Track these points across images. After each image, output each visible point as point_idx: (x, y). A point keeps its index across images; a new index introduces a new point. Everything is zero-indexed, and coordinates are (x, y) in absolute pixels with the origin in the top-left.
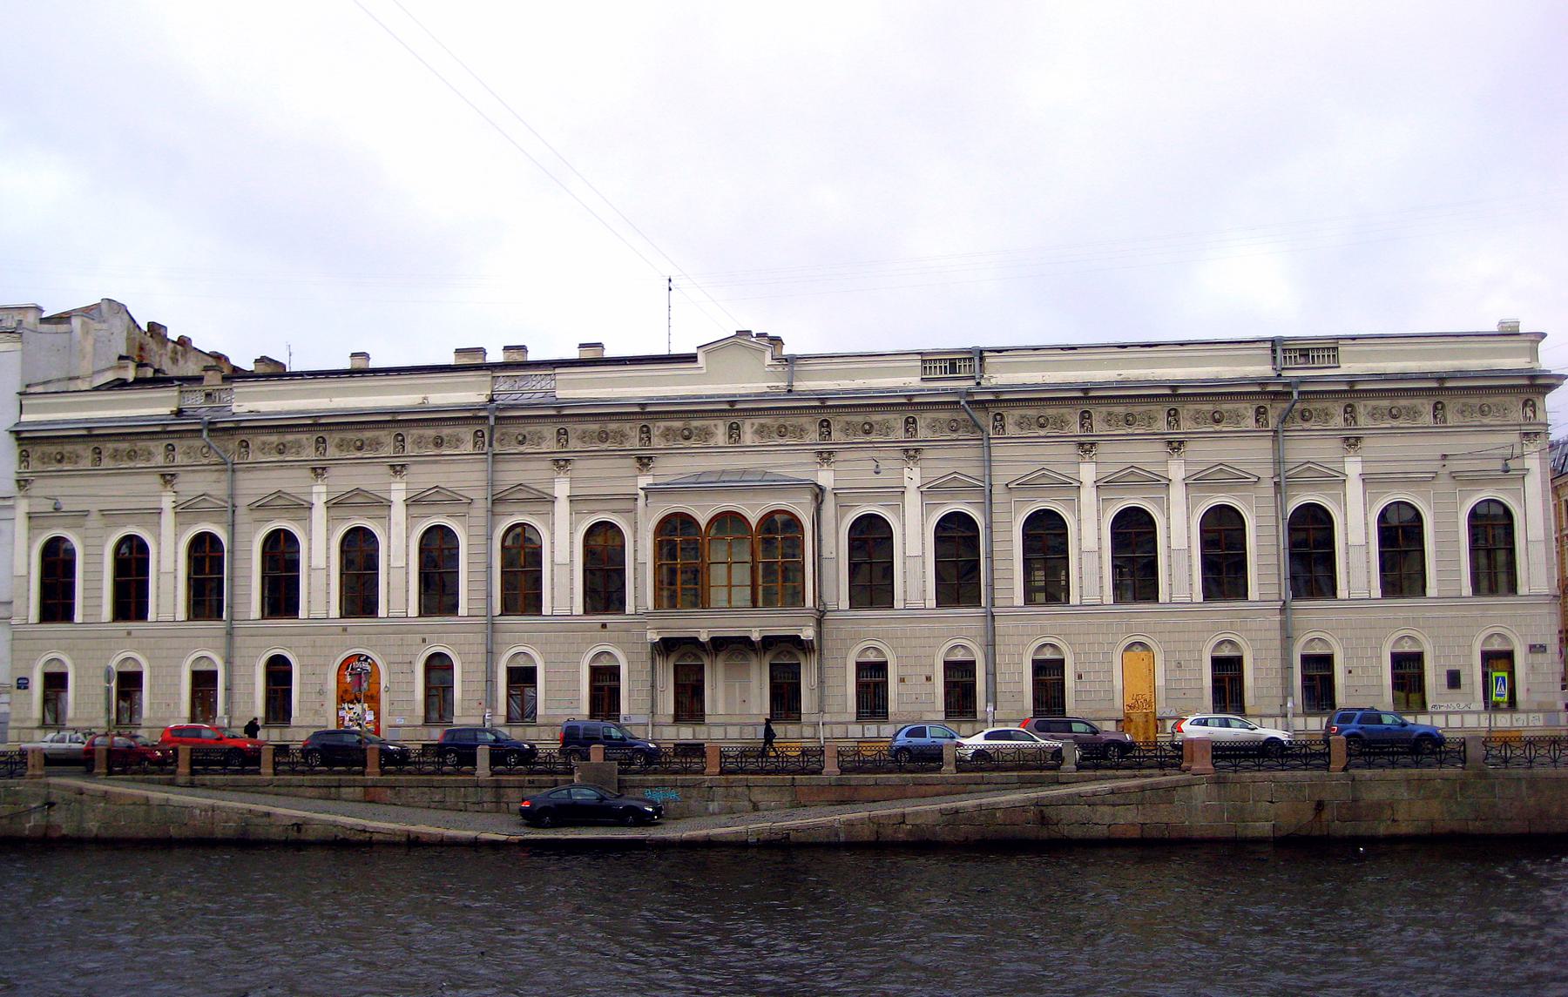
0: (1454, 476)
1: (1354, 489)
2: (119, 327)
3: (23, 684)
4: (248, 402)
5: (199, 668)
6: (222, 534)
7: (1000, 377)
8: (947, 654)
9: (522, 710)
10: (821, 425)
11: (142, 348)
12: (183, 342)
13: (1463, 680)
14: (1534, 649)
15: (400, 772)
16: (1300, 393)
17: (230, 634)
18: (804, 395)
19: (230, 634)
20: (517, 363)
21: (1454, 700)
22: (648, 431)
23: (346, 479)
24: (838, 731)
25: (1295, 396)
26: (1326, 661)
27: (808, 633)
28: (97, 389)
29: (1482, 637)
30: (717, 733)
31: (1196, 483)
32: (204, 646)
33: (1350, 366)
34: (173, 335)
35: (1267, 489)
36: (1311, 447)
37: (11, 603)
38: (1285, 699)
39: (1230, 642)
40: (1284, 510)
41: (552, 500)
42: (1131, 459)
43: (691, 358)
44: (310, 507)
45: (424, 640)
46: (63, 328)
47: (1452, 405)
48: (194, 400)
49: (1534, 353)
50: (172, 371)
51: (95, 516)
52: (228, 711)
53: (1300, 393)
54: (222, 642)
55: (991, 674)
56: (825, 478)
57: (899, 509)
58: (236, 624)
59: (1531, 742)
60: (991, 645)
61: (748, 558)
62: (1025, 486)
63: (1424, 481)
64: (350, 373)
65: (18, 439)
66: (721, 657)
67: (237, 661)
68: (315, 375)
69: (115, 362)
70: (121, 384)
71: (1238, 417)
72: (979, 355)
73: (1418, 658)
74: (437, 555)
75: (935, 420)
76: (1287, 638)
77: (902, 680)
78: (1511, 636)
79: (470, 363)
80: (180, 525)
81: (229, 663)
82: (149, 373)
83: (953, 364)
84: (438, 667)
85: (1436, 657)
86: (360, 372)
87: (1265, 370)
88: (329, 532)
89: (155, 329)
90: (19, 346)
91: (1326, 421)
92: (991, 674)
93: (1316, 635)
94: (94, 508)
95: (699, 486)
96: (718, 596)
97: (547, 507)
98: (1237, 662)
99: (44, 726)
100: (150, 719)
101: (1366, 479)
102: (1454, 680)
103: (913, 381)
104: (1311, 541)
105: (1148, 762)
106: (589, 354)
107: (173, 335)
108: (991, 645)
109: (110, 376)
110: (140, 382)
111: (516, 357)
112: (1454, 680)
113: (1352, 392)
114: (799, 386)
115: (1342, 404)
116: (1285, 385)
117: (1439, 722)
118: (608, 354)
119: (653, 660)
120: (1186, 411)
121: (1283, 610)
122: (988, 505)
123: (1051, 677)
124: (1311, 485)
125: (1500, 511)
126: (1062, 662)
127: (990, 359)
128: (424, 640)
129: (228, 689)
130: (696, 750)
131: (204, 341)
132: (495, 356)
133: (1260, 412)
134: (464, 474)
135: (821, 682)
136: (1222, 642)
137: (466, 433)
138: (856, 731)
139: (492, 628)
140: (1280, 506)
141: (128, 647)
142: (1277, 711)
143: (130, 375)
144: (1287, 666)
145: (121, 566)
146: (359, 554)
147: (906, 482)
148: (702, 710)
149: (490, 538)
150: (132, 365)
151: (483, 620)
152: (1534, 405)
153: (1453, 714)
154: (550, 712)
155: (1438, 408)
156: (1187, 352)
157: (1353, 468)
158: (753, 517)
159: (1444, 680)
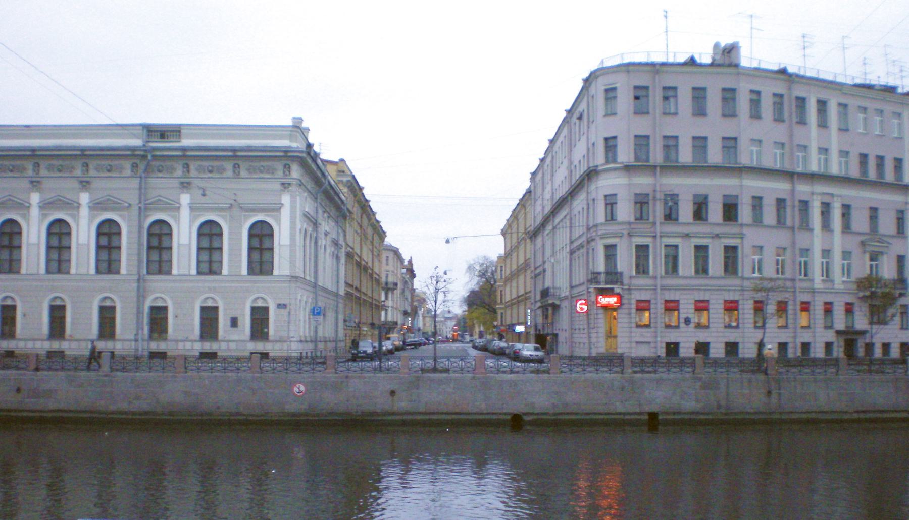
1: (185, 213)
5: (54, 303)
13: (239, 323)
14: (279, 306)
16: (153, 156)
21: (235, 335)
22: (87, 166)
24: (188, 345)
25: (150, 157)
29: (52, 296)
30: (22, 344)
31: (45, 206)
33: (186, 142)
35: (135, 211)
36: (162, 185)
38: (138, 331)
39: (60, 298)
44: (178, 209)
47: (244, 165)
59: (238, 359)
71: (121, 169)
73: (215, 309)
75: (200, 166)
77: (24, 315)
85: (225, 310)
87: (137, 142)
91: (71, 172)
93: (158, 295)
98: (63, 308)
101: (192, 208)
102: (234, 322)
104: (159, 239)
105: (579, 361)
112: (234, 322)
113: (186, 156)
115: (181, 162)
120: (92, 164)
124: (161, 210)
125: (259, 224)
126: (216, 308)
130: (212, 356)
133: (135, 166)
134: (124, 187)
136: (258, 298)
137: (127, 165)
142: (132, 337)
144: (139, 312)
148: (14, 332)
151: (136, 277)
152: (289, 168)
153: (235, 340)
155: (236, 167)
157: (84, 198)
159: (229, 323)
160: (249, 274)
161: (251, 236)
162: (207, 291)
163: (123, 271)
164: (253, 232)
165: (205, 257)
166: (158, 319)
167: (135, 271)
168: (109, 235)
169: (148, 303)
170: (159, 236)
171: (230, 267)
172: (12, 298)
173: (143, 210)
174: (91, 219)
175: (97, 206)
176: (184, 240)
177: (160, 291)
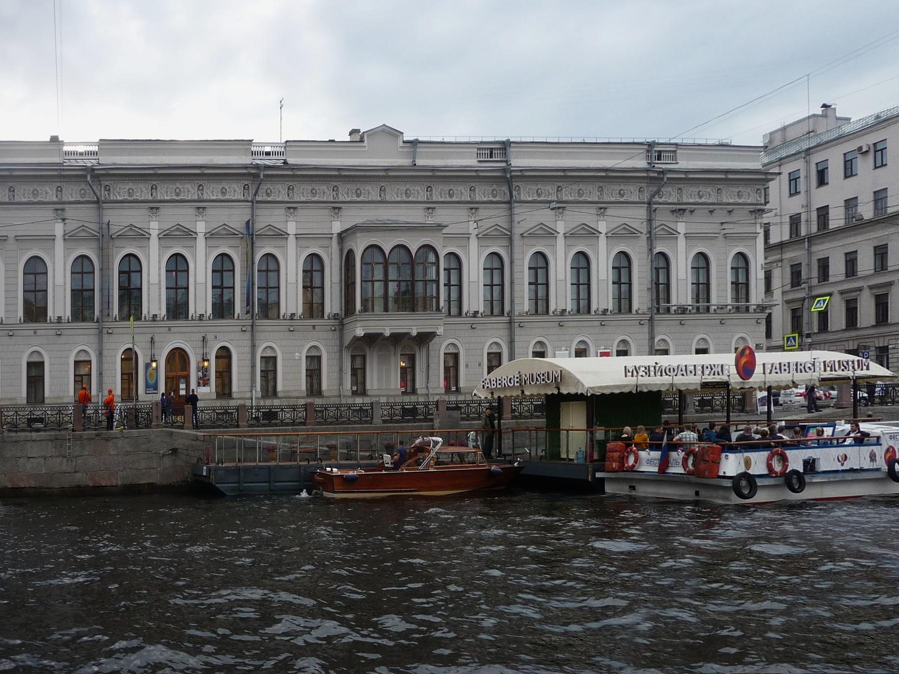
0: (725, 236)
6: (503, 252)
7: (518, 162)
8: (76, 356)
9: (269, 388)
10: (10, 190)
18: (424, 169)
23: (173, 217)
32: (81, 342)
33: (684, 164)
35: (643, 241)
39: (270, 347)
41: (53, 238)
42: (542, 220)
45: (216, 337)
51: (11, 241)
53: (668, 179)
54: (505, 333)
60: (511, 343)
62: (531, 235)
63: (712, 238)
67: (105, 353)
72: (505, 146)
77: (467, 366)
80: (67, 250)
81: (100, 354)
87: (642, 164)
88: (608, 253)
94: (11, 235)
97: (282, 243)
99: (355, 393)
100: (284, 391)
103: (471, 161)
114: (420, 162)
116: (659, 172)
121: (651, 319)
126: (42, 363)
127: (512, 150)
128: (216, 337)
136: (311, 347)
138: (218, 403)
145: (308, 273)
154: (287, 389)
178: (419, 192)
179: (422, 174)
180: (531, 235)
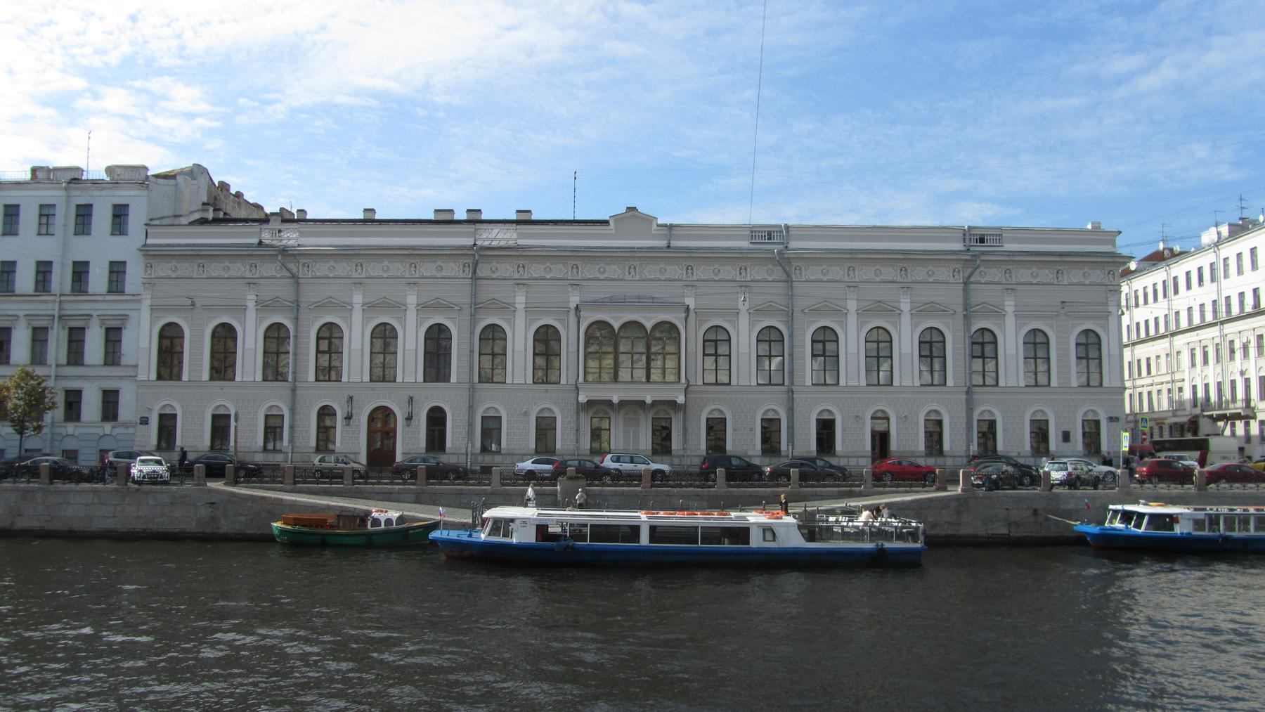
2: (203, 181)
3: (144, 421)
4: (291, 237)
6: (290, 325)
11: (215, 198)
12: (239, 195)
13: (1060, 434)
14: (1111, 419)
15: (366, 483)
17: (294, 390)
19: (294, 390)
20: (475, 220)
26: (992, 424)
27: (681, 399)
28: (192, 223)
29: (762, 411)
32: (276, 398)
33: (1008, 247)
34: (233, 191)
37: (136, 366)
40: (969, 330)
43: (606, 222)
46: (172, 182)
48: (266, 237)
49: (1113, 243)
50: (234, 215)
52: (291, 441)
55: (791, 428)
56: (690, 302)
57: (897, 325)
58: (298, 384)
60: (791, 411)
61: (644, 350)
64: (517, 222)
65: (146, 255)
66: (622, 412)
68: (556, 222)
69: (200, 207)
70: (203, 222)
74: (437, 340)
76: (471, 408)
77: (751, 430)
78: (833, 410)
79: (444, 220)
81: (293, 410)
82: (221, 215)
83: (769, 234)
84: (437, 419)
86: (369, 220)
87: (959, 246)
89: (224, 186)
90: (146, 193)
92: (791, 428)
95: (611, 303)
96: (624, 374)
98: (939, 423)
102: (1066, 437)
103: (745, 244)
104: (983, 346)
106: (523, 217)
107: (233, 191)
108: (791, 411)
109: (197, 216)
110: (216, 221)
111: (474, 216)
112: (1066, 437)
117: (843, 462)
118: (534, 217)
119: (578, 414)
121: (967, 392)
122: (790, 324)
123: (222, 423)
126: (175, 415)
129: (292, 427)
131: (250, 197)
132: (461, 215)
135: (685, 430)
139: (472, 389)
140: (473, 325)
141: (223, 398)
143: (210, 216)
144: (471, 424)
146: (384, 337)
147: (740, 305)
149: (472, 333)
150: (211, 209)
151: (467, 386)
156: (384, 228)
158: (649, 326)
160: (425, 381)
161: (214, 335)
162: (276, 398)
163: (454, 379)
164: (551, 331)
165: (541, 361)
166: (491, 429)
167: (466, 377)
168: (172, 339)
169: (976, 417)
170: (172, 339)
171: (1059, 378)
172: (830, 412)
173: (476, 308)
174: (860, 326)
175: (919, 312)
176: (356, 344)
177: (492, 401)
178: (675, 271)
179: (682, 251)
180: (816, 311)
